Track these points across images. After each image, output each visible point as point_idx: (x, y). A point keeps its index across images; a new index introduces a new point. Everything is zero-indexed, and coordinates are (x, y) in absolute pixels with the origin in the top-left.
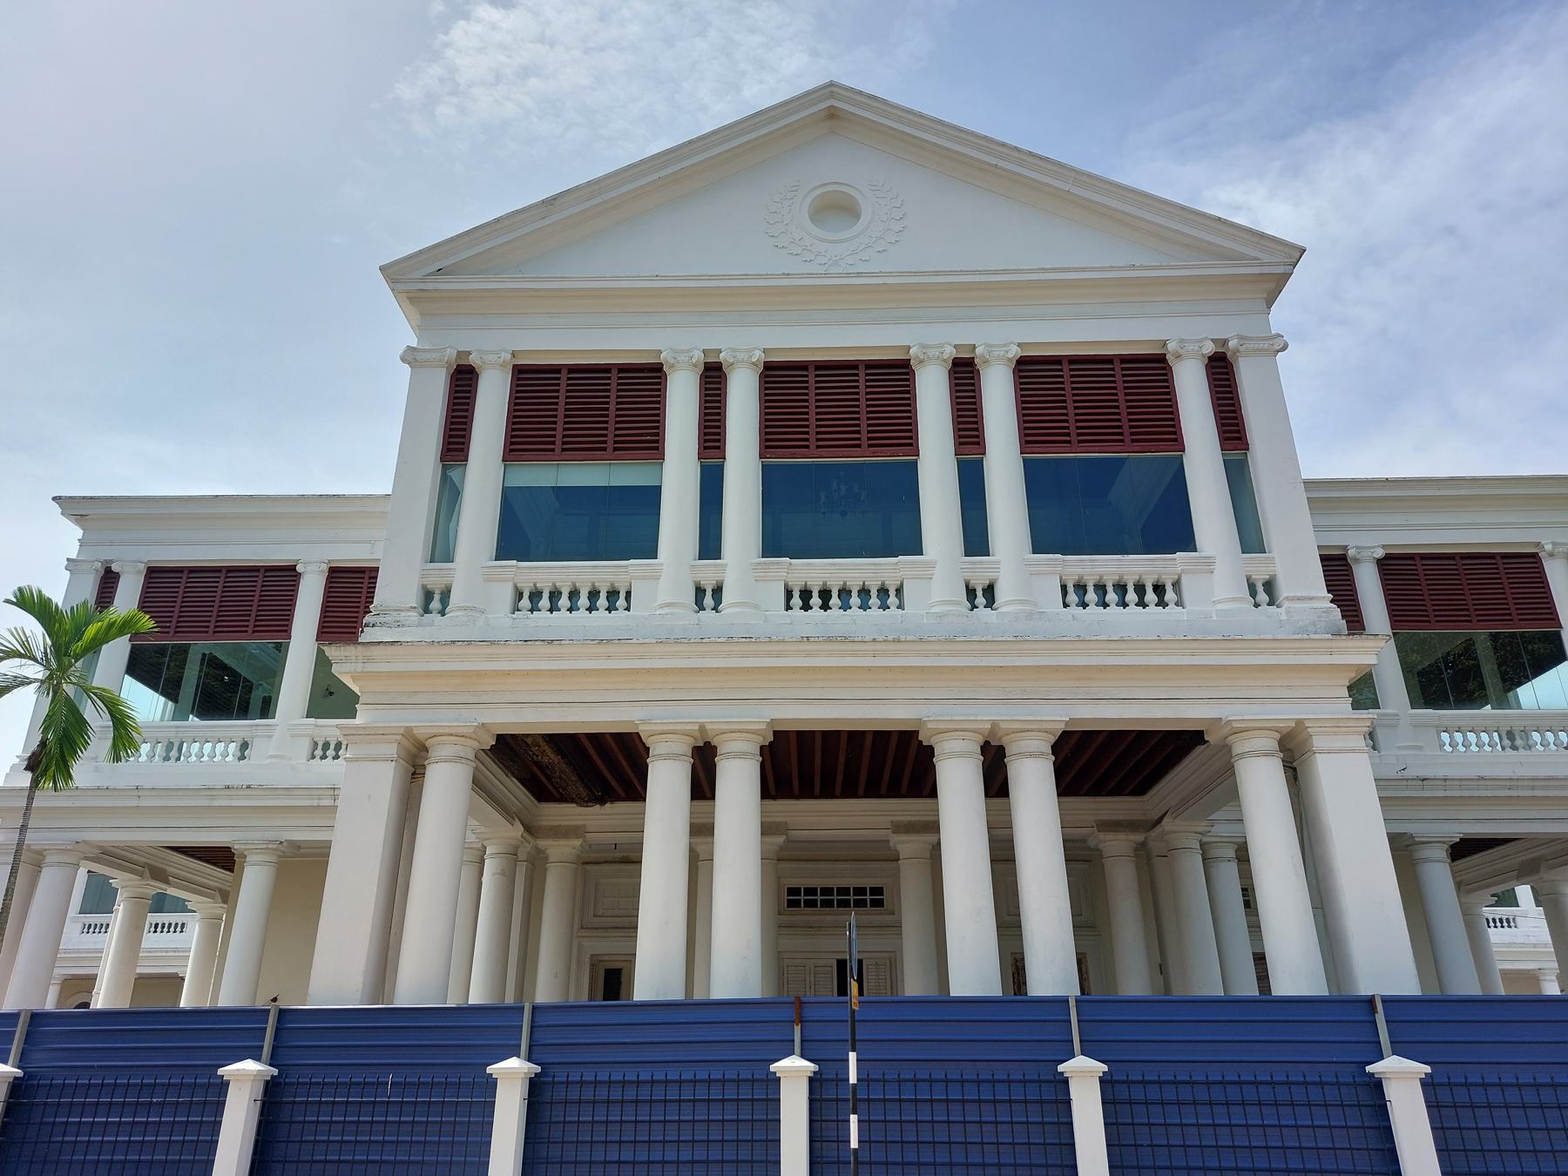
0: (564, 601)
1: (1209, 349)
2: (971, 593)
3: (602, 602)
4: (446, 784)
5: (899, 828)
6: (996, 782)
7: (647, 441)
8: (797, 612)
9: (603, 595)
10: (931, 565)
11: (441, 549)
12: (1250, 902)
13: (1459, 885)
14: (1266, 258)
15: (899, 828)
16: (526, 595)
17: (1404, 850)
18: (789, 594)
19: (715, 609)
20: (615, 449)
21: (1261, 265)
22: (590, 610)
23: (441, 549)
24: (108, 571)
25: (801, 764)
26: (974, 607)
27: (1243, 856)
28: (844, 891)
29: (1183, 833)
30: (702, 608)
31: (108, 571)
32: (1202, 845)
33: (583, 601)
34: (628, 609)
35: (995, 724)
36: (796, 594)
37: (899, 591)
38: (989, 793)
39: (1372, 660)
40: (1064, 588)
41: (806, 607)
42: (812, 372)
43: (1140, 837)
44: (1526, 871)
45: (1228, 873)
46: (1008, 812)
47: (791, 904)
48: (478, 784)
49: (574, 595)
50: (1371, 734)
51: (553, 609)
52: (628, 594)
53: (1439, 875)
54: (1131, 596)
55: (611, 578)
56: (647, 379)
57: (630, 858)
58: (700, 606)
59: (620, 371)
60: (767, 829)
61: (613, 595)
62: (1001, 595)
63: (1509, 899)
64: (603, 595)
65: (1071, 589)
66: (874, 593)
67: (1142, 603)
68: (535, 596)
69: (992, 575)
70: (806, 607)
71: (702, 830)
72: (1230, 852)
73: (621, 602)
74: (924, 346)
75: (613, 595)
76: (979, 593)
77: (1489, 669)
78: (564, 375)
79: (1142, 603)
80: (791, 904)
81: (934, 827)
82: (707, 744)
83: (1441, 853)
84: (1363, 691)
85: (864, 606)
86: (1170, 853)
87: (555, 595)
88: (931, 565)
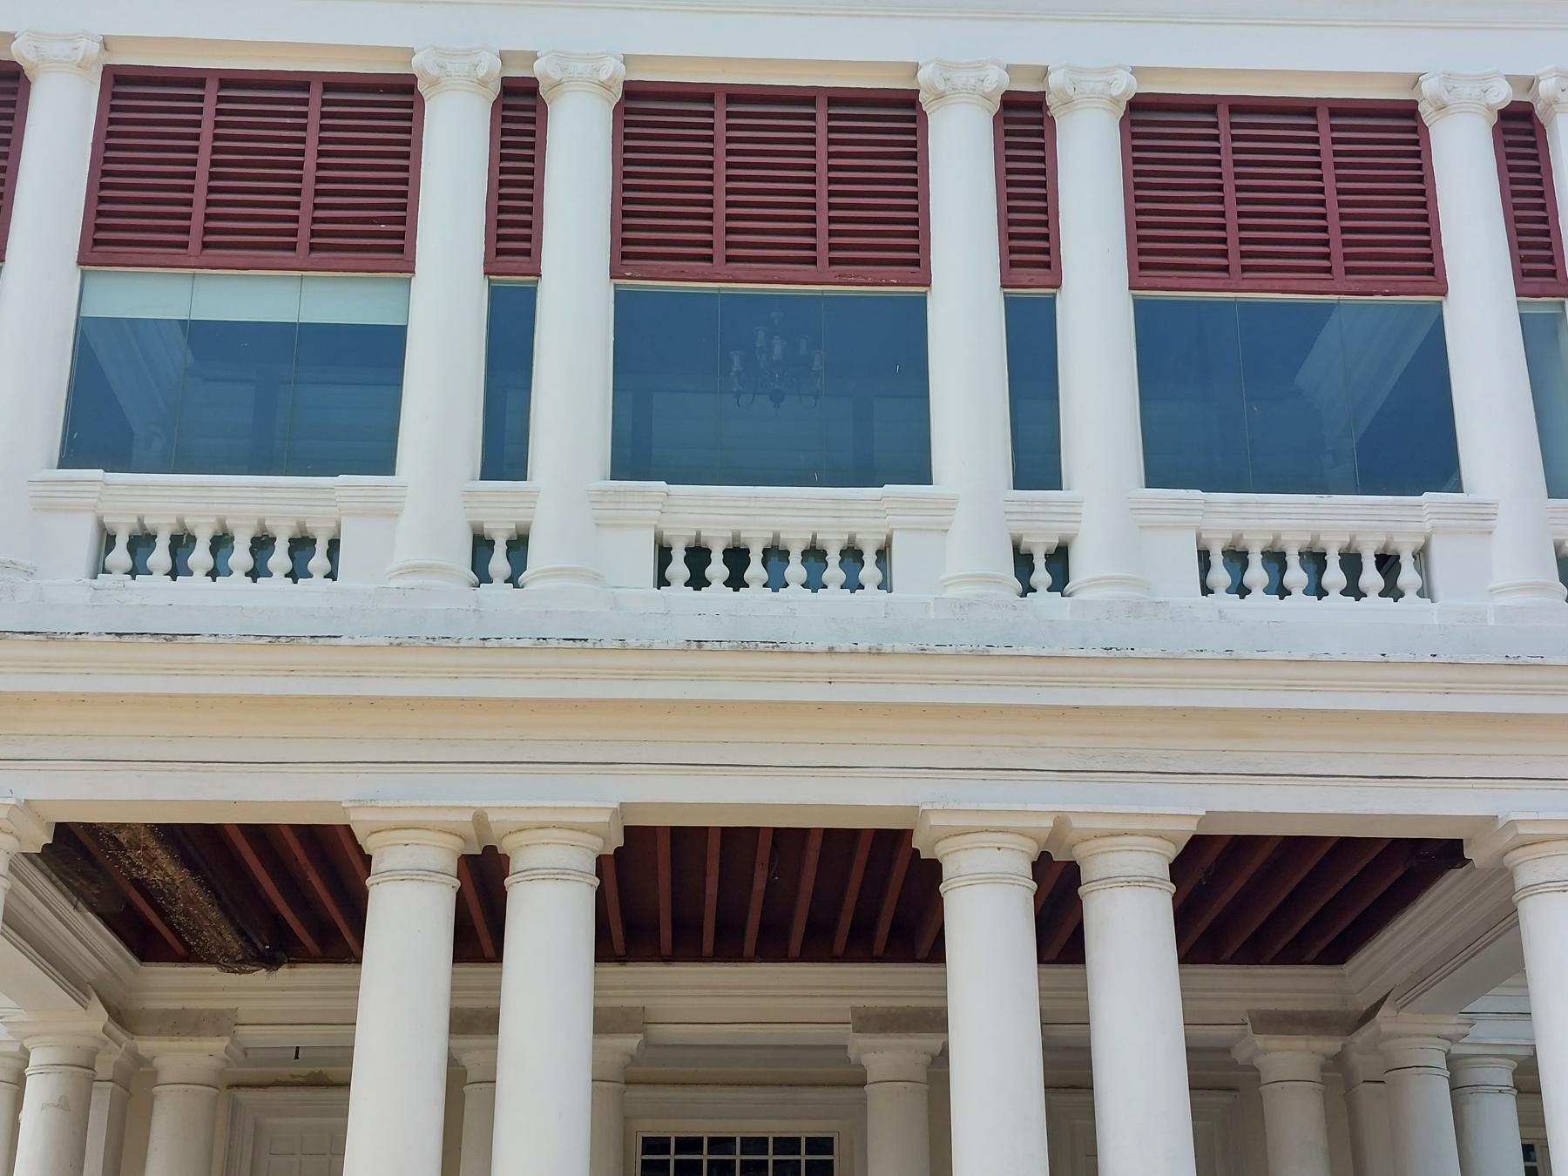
1: (1502, 95)
2: (1023, 562)
3: (279, 559)
7: (379, 232)
9: (282, 546)
10: (948, 505)
18: (664, 555)
19: (513, 580)
26: (1028, 589)
27: (1527, 1083)
29: (1416, 1036)
32: (1451, 1060)
33: (241, 557)
34: (332, 575)
35: (1061, 820)
37: (883, 555)
40: (1204, 557)
41: (698, 581)
43: (1332, 1045)
46: (1081, 991)
49: (221, 543)
51: (736, 581)
59: (327, 87)
60: (605, 1022)
61: (301, 545)
64: (282, 546)
68: (141, 543)
70: (698, 581)
72: (1504, 1077)
73: (319, 562)
76: (1040, 562)
79: (1353, 590)
82: (490, 850)
86: (1390, 1074)
87: (181, 543)
88: (948, 505)
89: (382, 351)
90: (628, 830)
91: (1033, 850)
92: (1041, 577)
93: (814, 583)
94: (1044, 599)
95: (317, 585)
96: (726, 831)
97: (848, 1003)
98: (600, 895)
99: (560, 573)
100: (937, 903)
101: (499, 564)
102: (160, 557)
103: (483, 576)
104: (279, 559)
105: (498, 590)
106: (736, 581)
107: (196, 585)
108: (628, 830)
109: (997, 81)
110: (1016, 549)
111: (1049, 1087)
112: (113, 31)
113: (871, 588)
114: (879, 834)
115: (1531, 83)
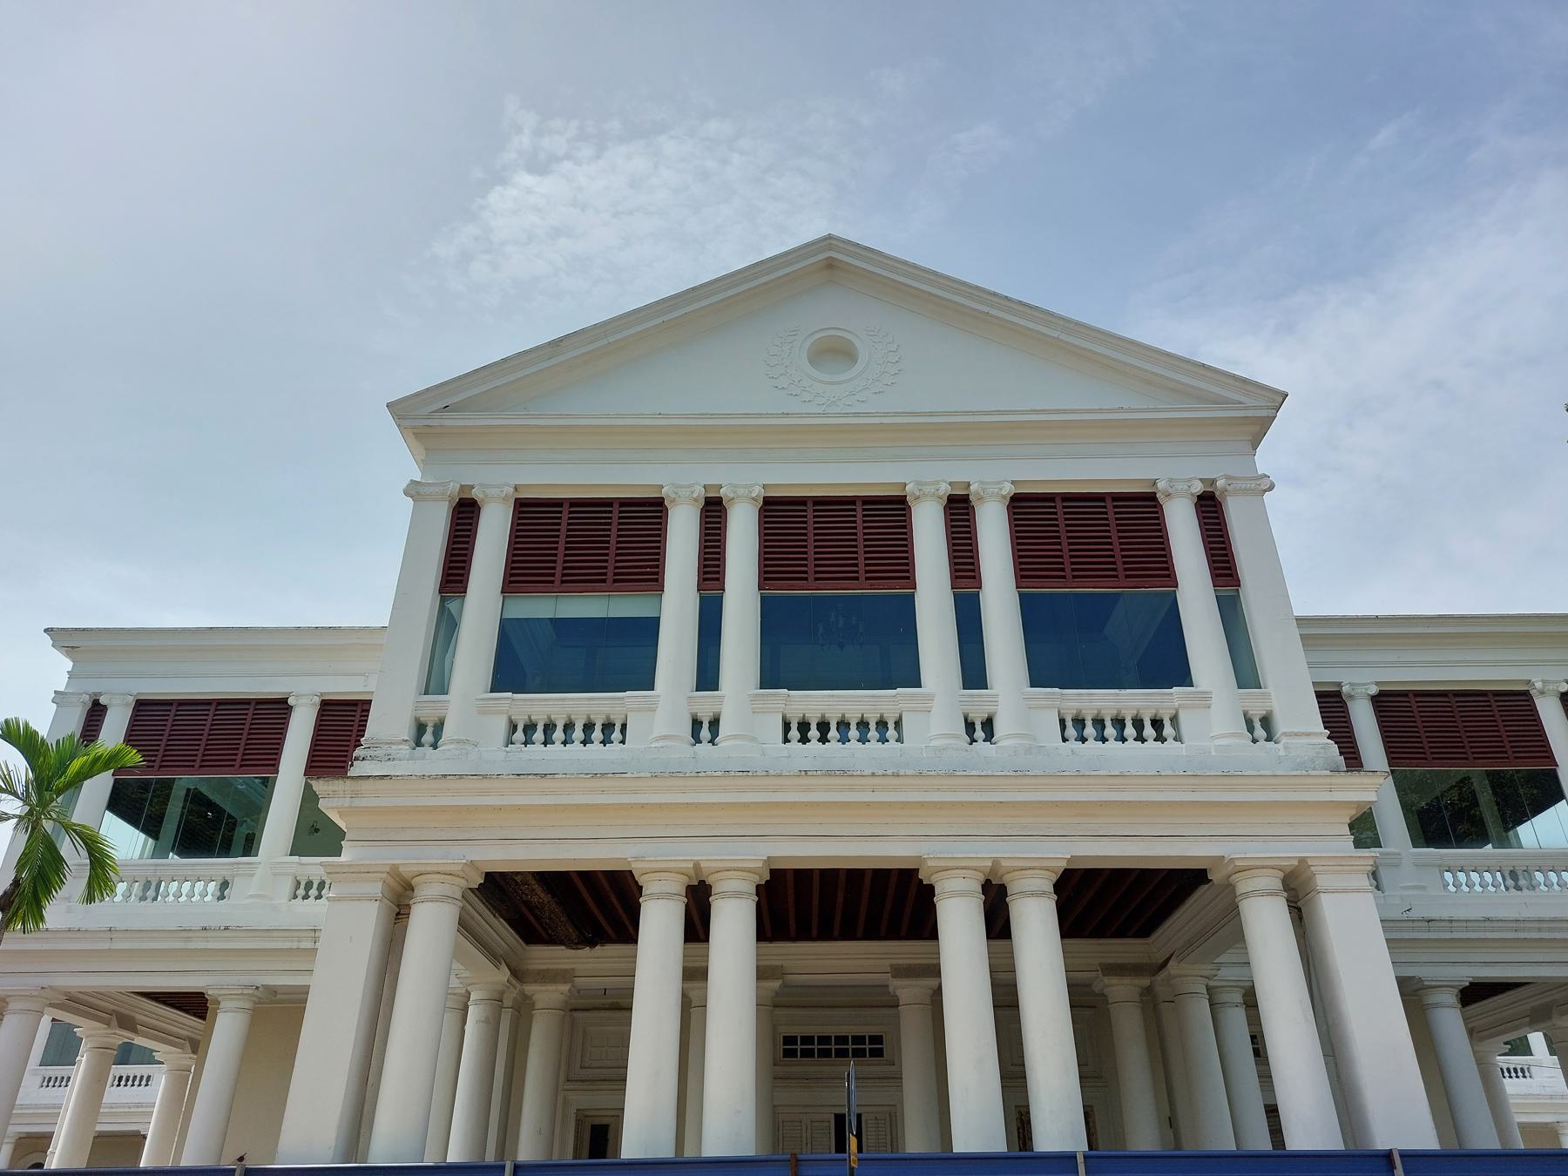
2: (970, 727)
3: (597, 734)
4: (432, 926)
8: (795, 745)
9: (598, 728)
11: (436, 681)
14: (1249, 402)
17: (1413, 994)
18: (787, 727)
19: (712, 741)
21: (1246, 408)
24: (96, 703)
26: (973, 741)
27: (1251, 1002)
28: (842, 1039)
29: (1190, 976)
30: (698, 741)
31: (96, 703)
32: (1208, 989)
35: (996, 861)
37: (898, 724)
38: (991, 935)
40: (1062, 722)
41: (804, 739)
45: (1236, 1019)
48: (464, 925)
51: (823, 739)
52: (624, 726)
55: (607, 710)
57: (620, 1005)
62: (1000, 728)
63: (1522, 1048)
64: (598, 728)
68: (530, 728)
72: (1238, 998)
75: (608, 727)
76: (978, 727)
80: (789, 1053)
82: (702, 882)
83: (1451, 998)
89: (648, 629)
90: (773, 872)
91: (982, 878)
92: (979, 734)
97: (888, 962)
98: (758, 905)
101: (705, 733)
104: (597, 734)
108: (773, 872)
109: (945, 490)
110: (1245, 715)
113: (892, 741)
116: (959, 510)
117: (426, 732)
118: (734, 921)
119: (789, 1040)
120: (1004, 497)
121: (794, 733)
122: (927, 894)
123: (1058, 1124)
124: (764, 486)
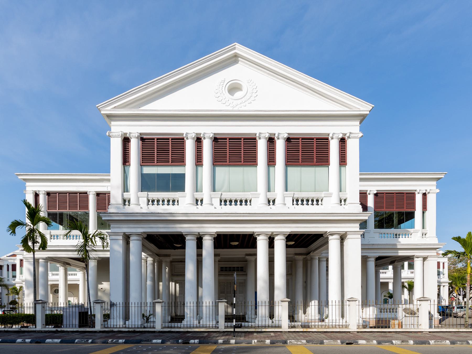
0: (161, 203)
1: (341, 136)
2: (269, 202)
3: (171, 203)
4: (135, 245)
5: (296, 254)
6: (200, 245)
7: (180, 160)
8: (223, 206)
9: (171, 201)
10: (259, 194)
11: (125, 189)
12: (327, 270)
13: (376, 266)
14: (362, 109)
15: (296, 254)
16: (150, 201)
17: (365, 260)
18: (221, 201)
19: (201, 205)
20: (172, 162)
21: (360, 111)
22: (168, 205)
23: (125, 189)
24: (36, 193)
25: (221, 241)
26: (270, 205)
27: (327, 261)
28: (234, 268)
29: (316, 255)
30: (270, 205)
31: (36, 193)
32: (319, 258)
33: (166, 202)
34: (129, 205)
35: (273, 232)
36: (223, 201)
37: (250, 201)
38: (269, 248)
39: (367, 218)
40: (293, 201)
41: (225, 205)
42: (315, 140)
43: (305, 257)
44: (392, 263)
45: (325, 263)
47: (221, 270)
48: (143, 245)
49: (163, 201)
50: (363, 235)
51: (241, 205)
52: (178, 201)
53: (371, 264)
54: (310, 202)
55: (173, 197)
56: (251, 141)
57: (183, 261)
58: (125, 205)
59: (317, 139)
60: (216, 255)
61: (174, 201)
62: (204, 202)
63: (57, 270)
64: (171, 201)
65: (295, 200)
66: (244, 201)
67: (302, 204)
68: (153, 201)
69: (275, 197)
70: (225, 205)
71: (199, 255)
72: (325, 259)
73: (176, 203)
74: (130, 133)
75: (174, 201)
76: (271, 201)
77: (395, 220)
78: (315, 140)
79: (302, 204)
80: (221, 270)
81: (255, 255)
82: (200, 237)
83: (373, 259)
84: (363, 224)
85: (231, 205)
86: (312, 259)
87: (158, 201)
88: (259, 194)
89: (182, 176)
91: (269, 236)
92: (271, 203)
93: (236, 205)
94: (271, 206)
95: (176, 206)
96: (223, 235)
99: (133, 204)
100: (256, 242)
102: (156, 203)
103: (125, 205)
104: (171, 203)
105: (199, 206)
106: (231, 205)
107: (161, 206)
111: (185, 262)
112: (280, 132)
113: (249, 205)
114: (249, 235)
115: (345, 135)
116: (271, 141)
117: (125, 202)
118: (208, 243)
119: (221, 268)
120: (211, 138)
121: (223, 203)
122: (255, 240)
123: (171, 283)
124: (214, 134)
